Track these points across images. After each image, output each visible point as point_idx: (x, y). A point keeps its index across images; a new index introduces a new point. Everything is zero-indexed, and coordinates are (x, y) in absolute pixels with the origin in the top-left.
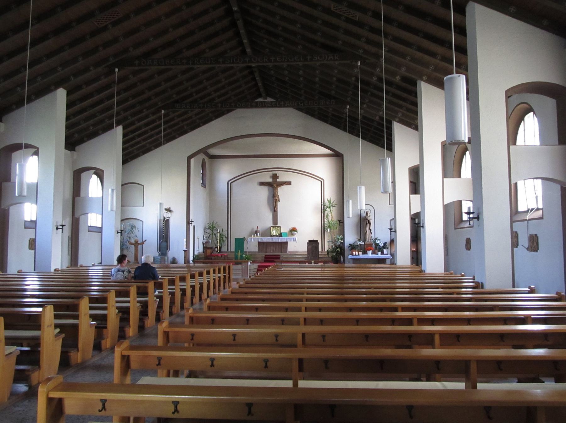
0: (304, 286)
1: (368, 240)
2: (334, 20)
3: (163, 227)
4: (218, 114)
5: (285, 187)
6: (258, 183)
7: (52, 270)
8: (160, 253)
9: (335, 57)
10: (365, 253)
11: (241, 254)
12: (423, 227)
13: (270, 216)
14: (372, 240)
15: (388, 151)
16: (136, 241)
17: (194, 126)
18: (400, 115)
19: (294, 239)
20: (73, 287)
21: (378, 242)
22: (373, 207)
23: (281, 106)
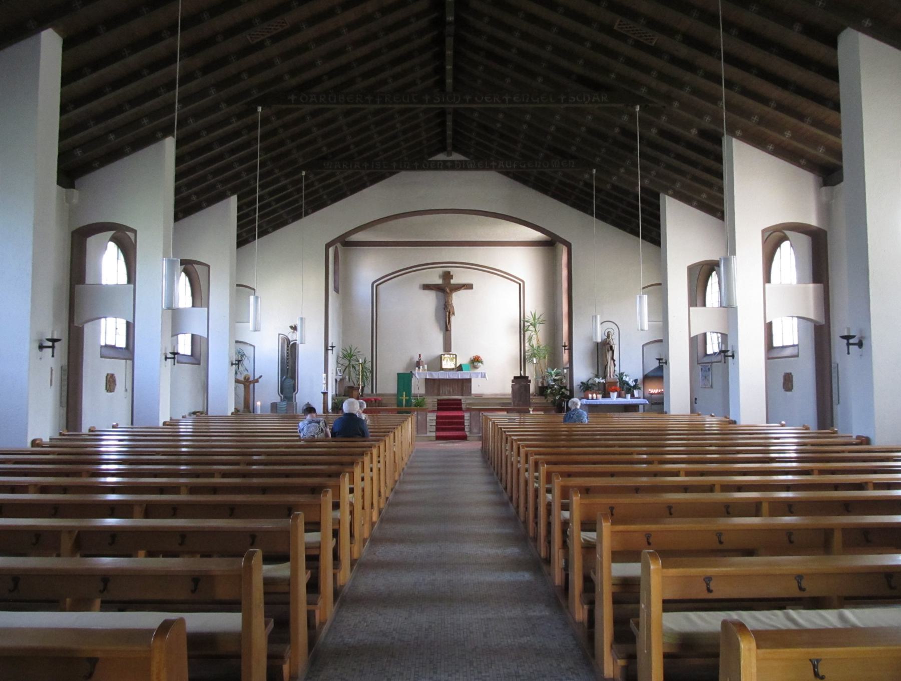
0: (829, 457)
2: (612, 43)
3: (288, 356)
4: (376, 178)
5: (462, 293)
6: (420, 285)
7: (161, 424)
8: (282, 396)
9: (603, 97)
10: (606, 395)
11: (407, 398)
12: (733, 356)
14: (616, 375)
15: (644, 241)
16: (247, 378)
17: (338, 195)
18: (678, 185)
19: (483, 375)
21: (627, 379)
22: (614, 323)
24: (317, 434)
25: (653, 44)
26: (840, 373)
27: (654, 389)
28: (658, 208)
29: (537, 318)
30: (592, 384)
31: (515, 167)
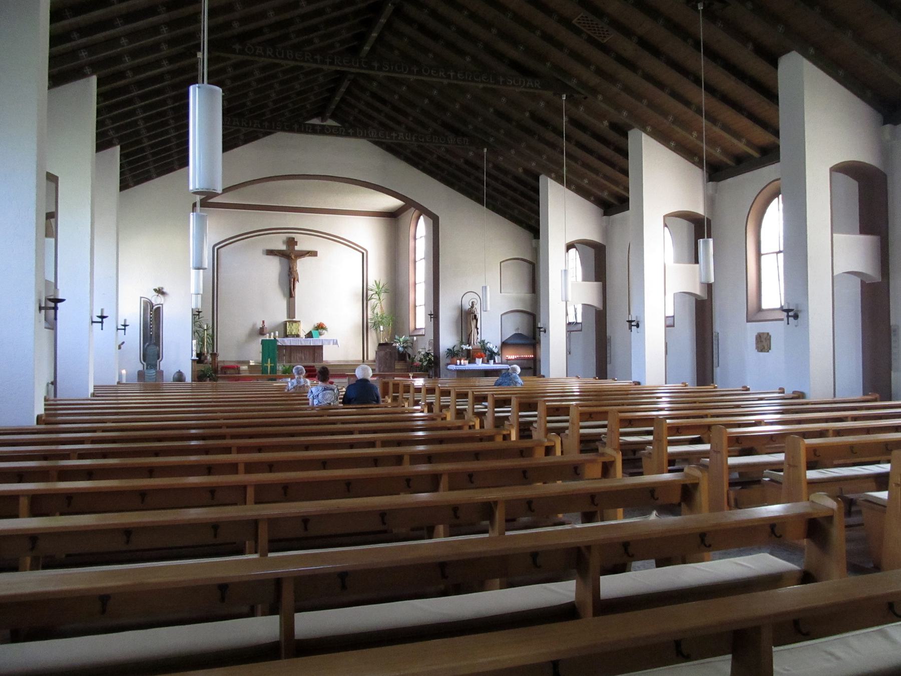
1: (474, 343)
5: (307, 260)
6: (263, 251)
10: (472, 361)
11: (272, 365)
13: (283, 303)
19: (335, 341)
20: (381, 414)
23: (347, 135)
24: (333, 402)
25: (605, 41)
26: (719, 341)
27: (510, 355)
28: (537, 191)
29: (381, 287)
30: (458, 351)
31: (414, 139)
